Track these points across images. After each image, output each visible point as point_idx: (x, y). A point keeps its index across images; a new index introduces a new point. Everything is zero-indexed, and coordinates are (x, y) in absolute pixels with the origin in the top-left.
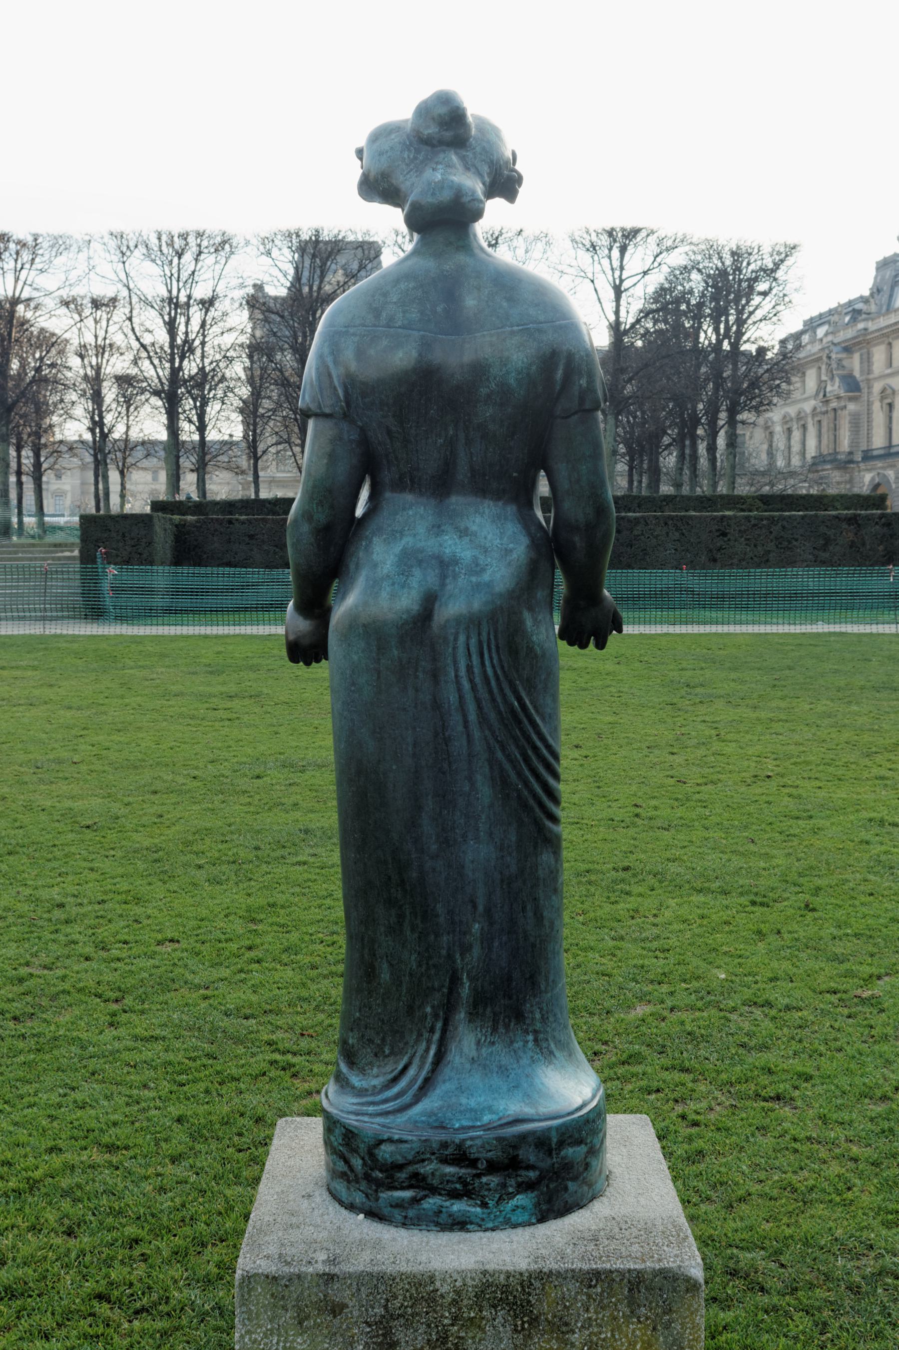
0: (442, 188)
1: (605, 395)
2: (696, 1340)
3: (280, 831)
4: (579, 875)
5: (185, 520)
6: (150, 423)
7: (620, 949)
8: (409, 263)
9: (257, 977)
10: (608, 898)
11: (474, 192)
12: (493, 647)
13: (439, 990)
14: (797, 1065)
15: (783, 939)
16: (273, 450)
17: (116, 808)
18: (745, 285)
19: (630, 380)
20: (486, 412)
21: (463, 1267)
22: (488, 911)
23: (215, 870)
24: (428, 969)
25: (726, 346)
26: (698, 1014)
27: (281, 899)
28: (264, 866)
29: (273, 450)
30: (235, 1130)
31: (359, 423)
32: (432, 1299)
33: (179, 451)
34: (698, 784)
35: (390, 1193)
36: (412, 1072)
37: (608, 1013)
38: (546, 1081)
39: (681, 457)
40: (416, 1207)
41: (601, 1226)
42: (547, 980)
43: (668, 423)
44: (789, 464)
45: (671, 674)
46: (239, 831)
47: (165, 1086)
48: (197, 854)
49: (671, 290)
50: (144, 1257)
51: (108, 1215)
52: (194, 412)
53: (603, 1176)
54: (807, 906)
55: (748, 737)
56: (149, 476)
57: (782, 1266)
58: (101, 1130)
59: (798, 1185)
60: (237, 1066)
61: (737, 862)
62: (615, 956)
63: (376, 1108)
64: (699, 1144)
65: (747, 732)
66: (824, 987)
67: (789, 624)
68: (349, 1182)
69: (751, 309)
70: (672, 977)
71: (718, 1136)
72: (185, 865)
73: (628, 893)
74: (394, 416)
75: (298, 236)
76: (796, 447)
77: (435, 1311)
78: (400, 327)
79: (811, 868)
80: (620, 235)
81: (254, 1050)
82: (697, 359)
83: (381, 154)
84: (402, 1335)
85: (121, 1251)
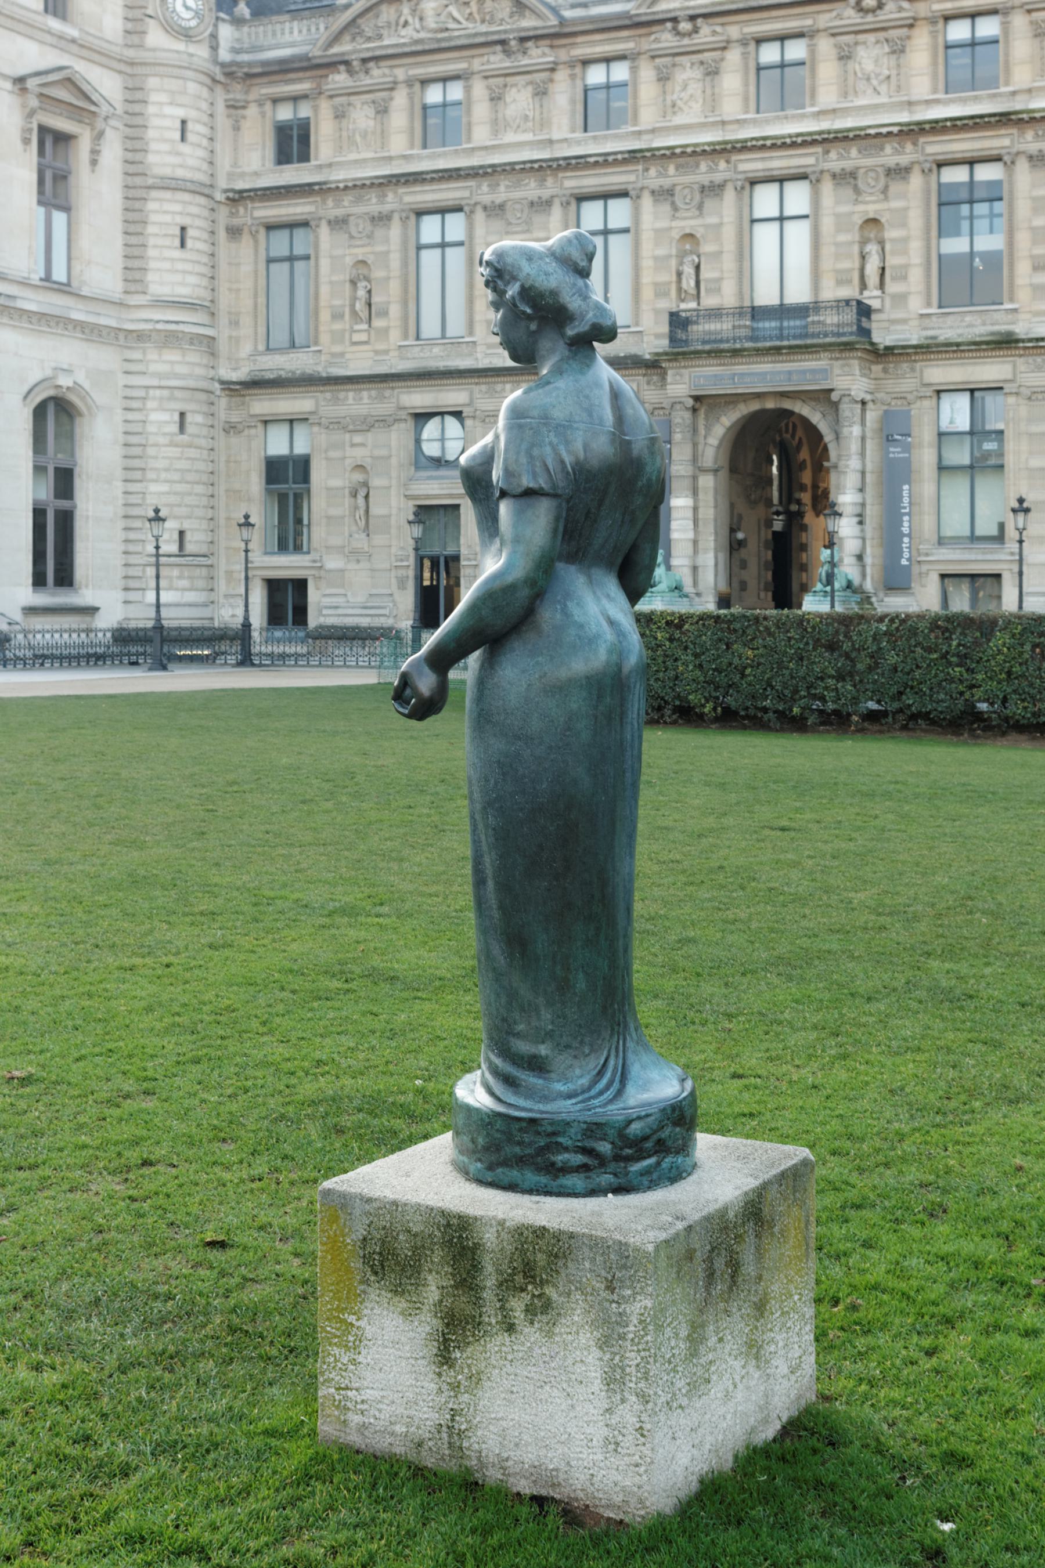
36: (612, 1062)
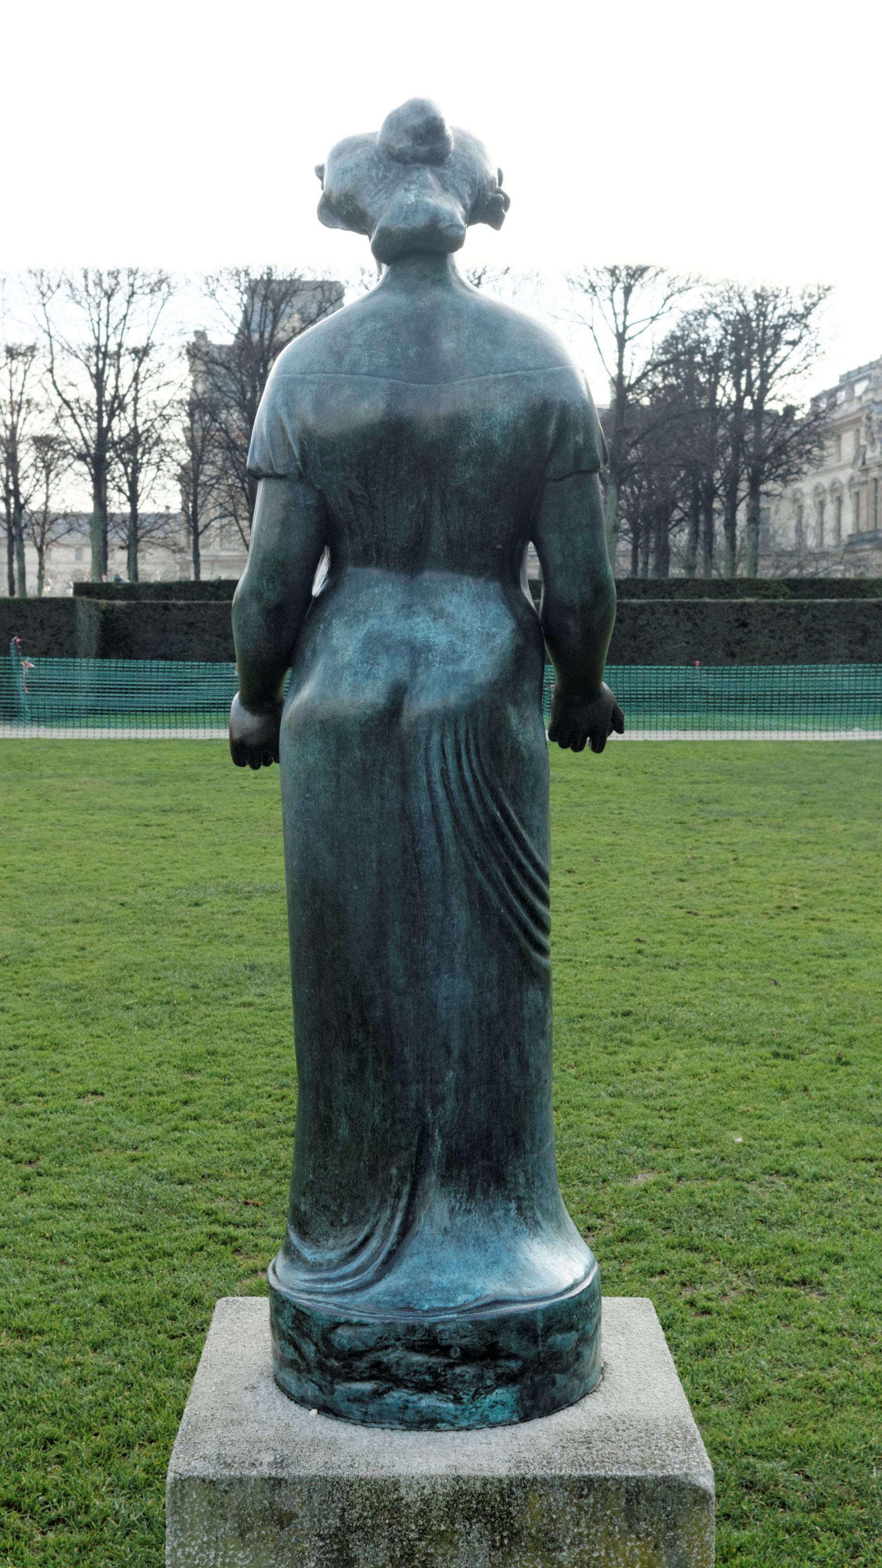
0: (416, 211)
1: (605, 454)
4: (571, 1020)
5: (113, 606)
6: (72, 492)
7: (618, 1107)
8: (377, 299)
9: (193, 1136)
10: (606, 1047)
11: (453, 216)
12: (472, 747)
13: (407, 1149)
14: (825, 1244)
15: (810, 1097)
16: (216, 524)
17: (31, 939)
18: (770, 332)
19: (634, 444)
21: (433, 1472)
22: (465, 1059)
23: (146, 1012)
24: (394, 1123)
25: (748, 404)
27: (221, 1046)
28: (203, 1008)
29: (216, 524)
30: (167, 1313)
31: (318, 486)
32: (396, 1509)
33: (106, 525)
34: (711, 917)
35: (347, 1385)
36: (374, 1244)
37: (604, 1181)
38: (531, 1256)
39: (695, 534)
40: (378, 1401)
41: (594, 1426)
42: (533, 1139)
43: (679, 494)
44: (821, 543)
45: (681, 788)
47: (87, 1262)
48: (124, 992)
49: (683, 339)
50: (61, 1460)
51: (19, 1410)
52: (124, 479)
53: (597, 1369)
54: (839, 1059)
55: (771, 862)
56: (71, 554)
57: (808, 1478)
58: (11, 1312)
59: (827, 1384)
60: (169, 1239)
61: (757, 1007)
62: (612, 1115)
63: (331, 1286)
64: (711, 1335)
65: (770, 856)
66: (858, 1153)
67: (821, 730)
68: (299, 1371)
69: (778, 361)
70: (679, 1140)
71: (732, 1326)
72: (112, 1006)
73: (629, 1043)
74: (358, 478)
75: (247, 274)
76: (830, 524)
78: (365, 374)
79: (844, 1014)
80: (624, 273)
81: (190, 1220)
82: (714, 419)
83: (344, 172)
84: (360, 1551)
85: (33, 1452)
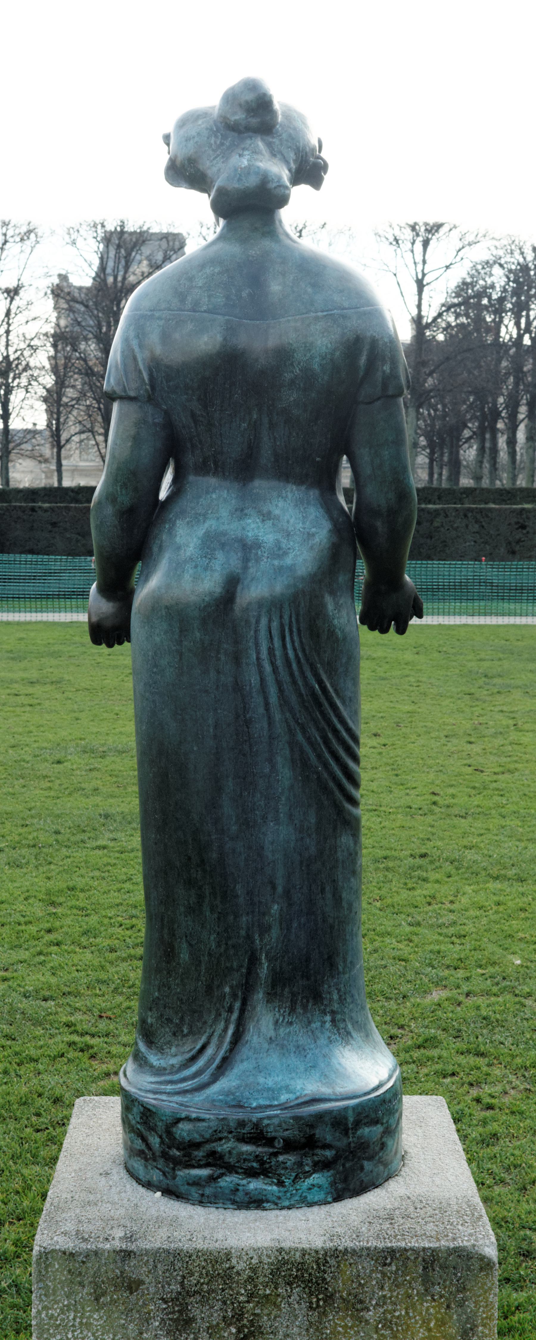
0: (249, 173)
2: (490, 1318)
3: (80, 816)
4: (376, 861)
7: (417, 934)
11: (280, 178)
12: (295, 630)
13: (238, 971)
16: (76, 439)
19: (431, 374)
20: (290, 397)
21: (259, 1245)
22: (287, 893)
23: (15, 854)
24: (226, 950)
26: (493, 999)
29: (76, 439)
31: (164, 407)
32: (228, 1276)
34: (495, 773)
35: (187, 1171)
36: (210, 1051)
37: (404, 997)
38: (343, 1061)
39: (482, 450)
40: (213, 1185)
41: (396, 1205)
42: (345, 961)
43: (468, 416)
45: (470, 665)
46: (39, 815)
49: (473, 285)
53: (399, 1156)
60: (35, 1047)
62: (411, 941)
63: (173, 1087)
64: (494, 1127)
68: (146, 1160)
70: (468, 962)
71: (512, 1119)
73: (425, 880)
74: (199, 399)
75: (103, 226)
77: (230, 1288)
78: (205, 311)
80: (423, 229)
81: (53, 1031)
82: (498, 353)
83: (188, 139)
84: (198, 1312)
